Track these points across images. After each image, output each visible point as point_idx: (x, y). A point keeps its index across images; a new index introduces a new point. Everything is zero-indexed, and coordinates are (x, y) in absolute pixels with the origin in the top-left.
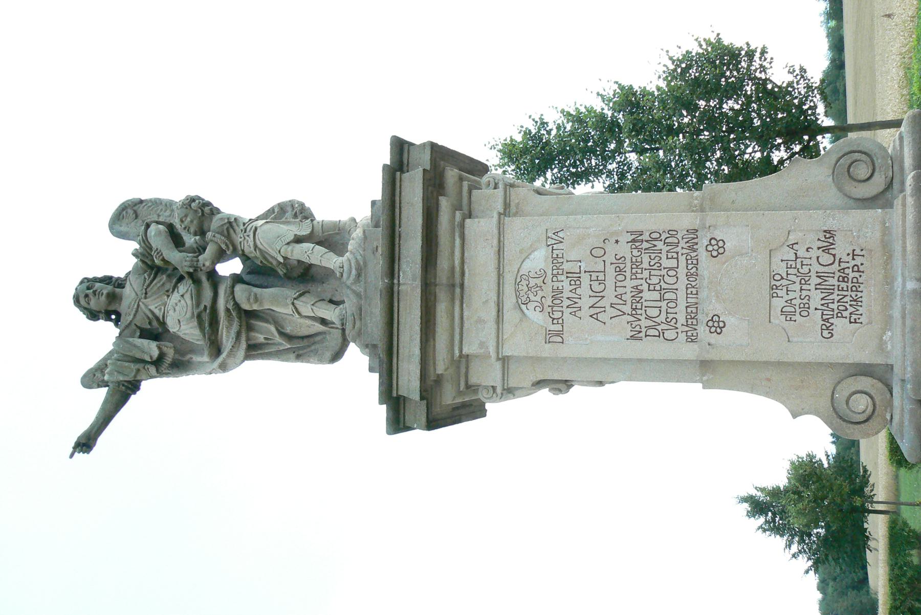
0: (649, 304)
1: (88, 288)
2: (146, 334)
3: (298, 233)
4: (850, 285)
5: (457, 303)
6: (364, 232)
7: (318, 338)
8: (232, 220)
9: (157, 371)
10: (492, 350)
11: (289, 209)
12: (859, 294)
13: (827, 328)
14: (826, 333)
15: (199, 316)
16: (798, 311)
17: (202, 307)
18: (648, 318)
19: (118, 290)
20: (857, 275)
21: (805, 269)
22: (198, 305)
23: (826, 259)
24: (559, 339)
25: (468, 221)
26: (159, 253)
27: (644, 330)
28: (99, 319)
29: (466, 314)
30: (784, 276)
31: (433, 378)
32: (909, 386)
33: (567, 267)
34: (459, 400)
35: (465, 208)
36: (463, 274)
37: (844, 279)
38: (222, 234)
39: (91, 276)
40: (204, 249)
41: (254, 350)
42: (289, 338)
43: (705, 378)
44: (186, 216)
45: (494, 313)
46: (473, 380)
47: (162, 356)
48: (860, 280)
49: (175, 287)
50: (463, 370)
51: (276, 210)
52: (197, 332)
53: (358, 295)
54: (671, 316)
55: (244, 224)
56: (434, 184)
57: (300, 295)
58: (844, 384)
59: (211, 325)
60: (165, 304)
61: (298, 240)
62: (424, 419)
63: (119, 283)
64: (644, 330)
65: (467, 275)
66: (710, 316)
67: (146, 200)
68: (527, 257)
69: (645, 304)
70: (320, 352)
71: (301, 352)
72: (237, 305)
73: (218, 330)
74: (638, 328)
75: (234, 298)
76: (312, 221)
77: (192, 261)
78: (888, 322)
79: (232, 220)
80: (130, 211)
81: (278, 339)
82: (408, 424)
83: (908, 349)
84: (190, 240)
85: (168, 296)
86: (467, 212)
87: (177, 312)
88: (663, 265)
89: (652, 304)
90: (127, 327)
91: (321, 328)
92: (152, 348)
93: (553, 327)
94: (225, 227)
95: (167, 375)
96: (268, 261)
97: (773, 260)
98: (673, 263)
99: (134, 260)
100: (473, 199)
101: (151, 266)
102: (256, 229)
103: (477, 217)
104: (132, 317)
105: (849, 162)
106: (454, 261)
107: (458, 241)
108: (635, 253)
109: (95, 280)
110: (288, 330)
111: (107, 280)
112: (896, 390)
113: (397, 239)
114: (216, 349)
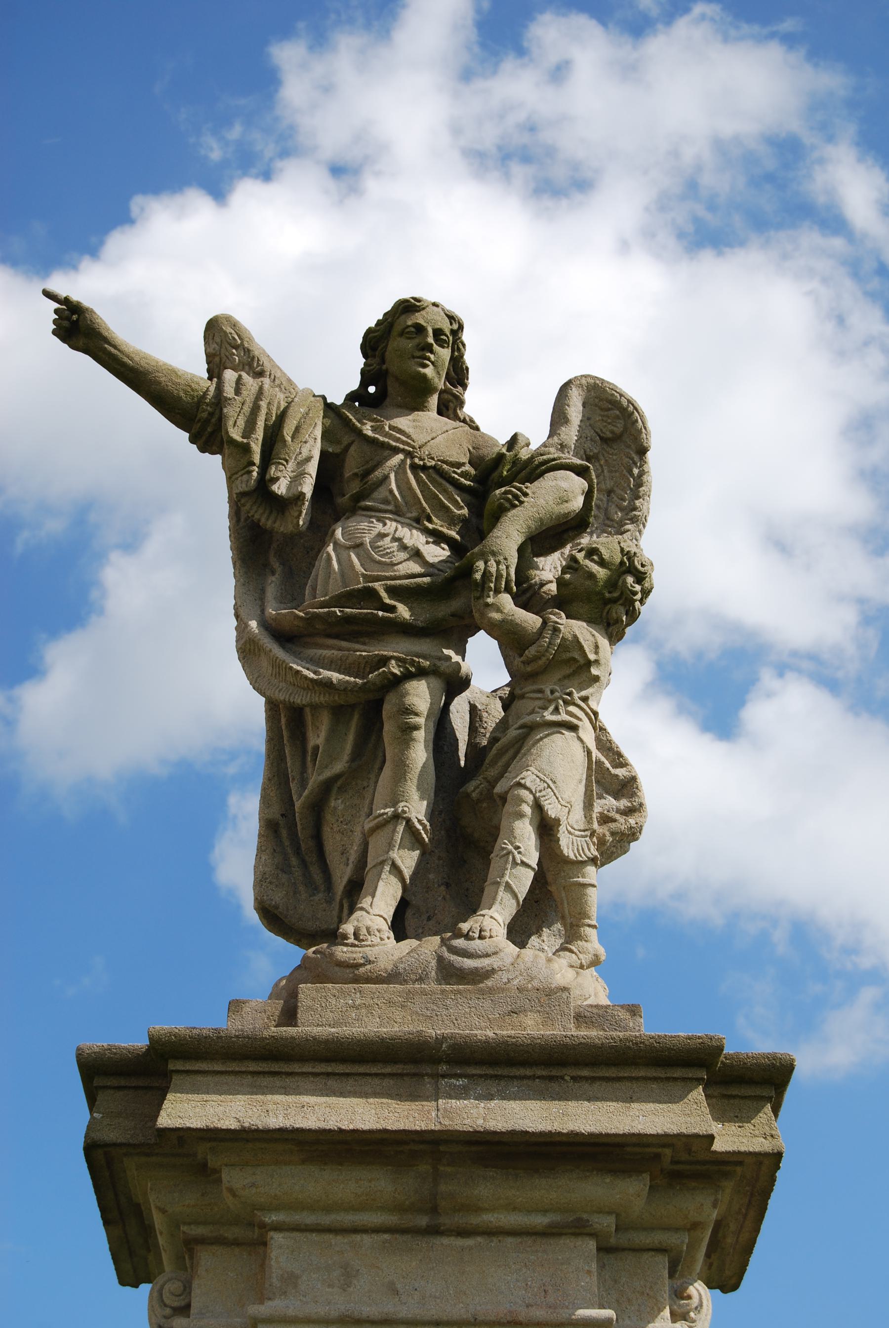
3: (562, 829)
5: (391, 1219)
6: (565, 989)
8: (594, 671)
9: (243, 494)
11: (624, 803)
26: (514, 502)
28: (365, 355)
31: (213, 1162)
34: (158, 1221)
35: (623, 1239)
36: (463, 1233)
40: (525, 606)
42: (318, 807)
44: (602, 563)
46: (206, 1258)
47: (284, 505)
50: (232, 1233)
55: (585, 699)
56: (680, 1164)
61: (546, 829)
62: (111, 1135)
63: (450, 406)
65: (460, 1242)
67: (643, 461)
70: (284, 878)
71: (284, 833)
72: (396, 682)
73: (337, 637)
76: (593, 861)
79: (594, 671)
80: (619, 427)
81: (315, 779)
82: (101, 1097)
84: (549, 569)
86: (613, 1241)
90: (347, 422)
91: (341, 882)
94: (576, 655)
95: (236, 513)
96: (494, 762)
99: (503, 438)
100: (646, 1256)
101: (497, 475)
102: (573, 728)
103: (602, 1267)
106: (492, 1210)
107: (540, 1221)
110: (337, 803)
111: (458, 374)
113: (540, 1072)
114: (286, 636)
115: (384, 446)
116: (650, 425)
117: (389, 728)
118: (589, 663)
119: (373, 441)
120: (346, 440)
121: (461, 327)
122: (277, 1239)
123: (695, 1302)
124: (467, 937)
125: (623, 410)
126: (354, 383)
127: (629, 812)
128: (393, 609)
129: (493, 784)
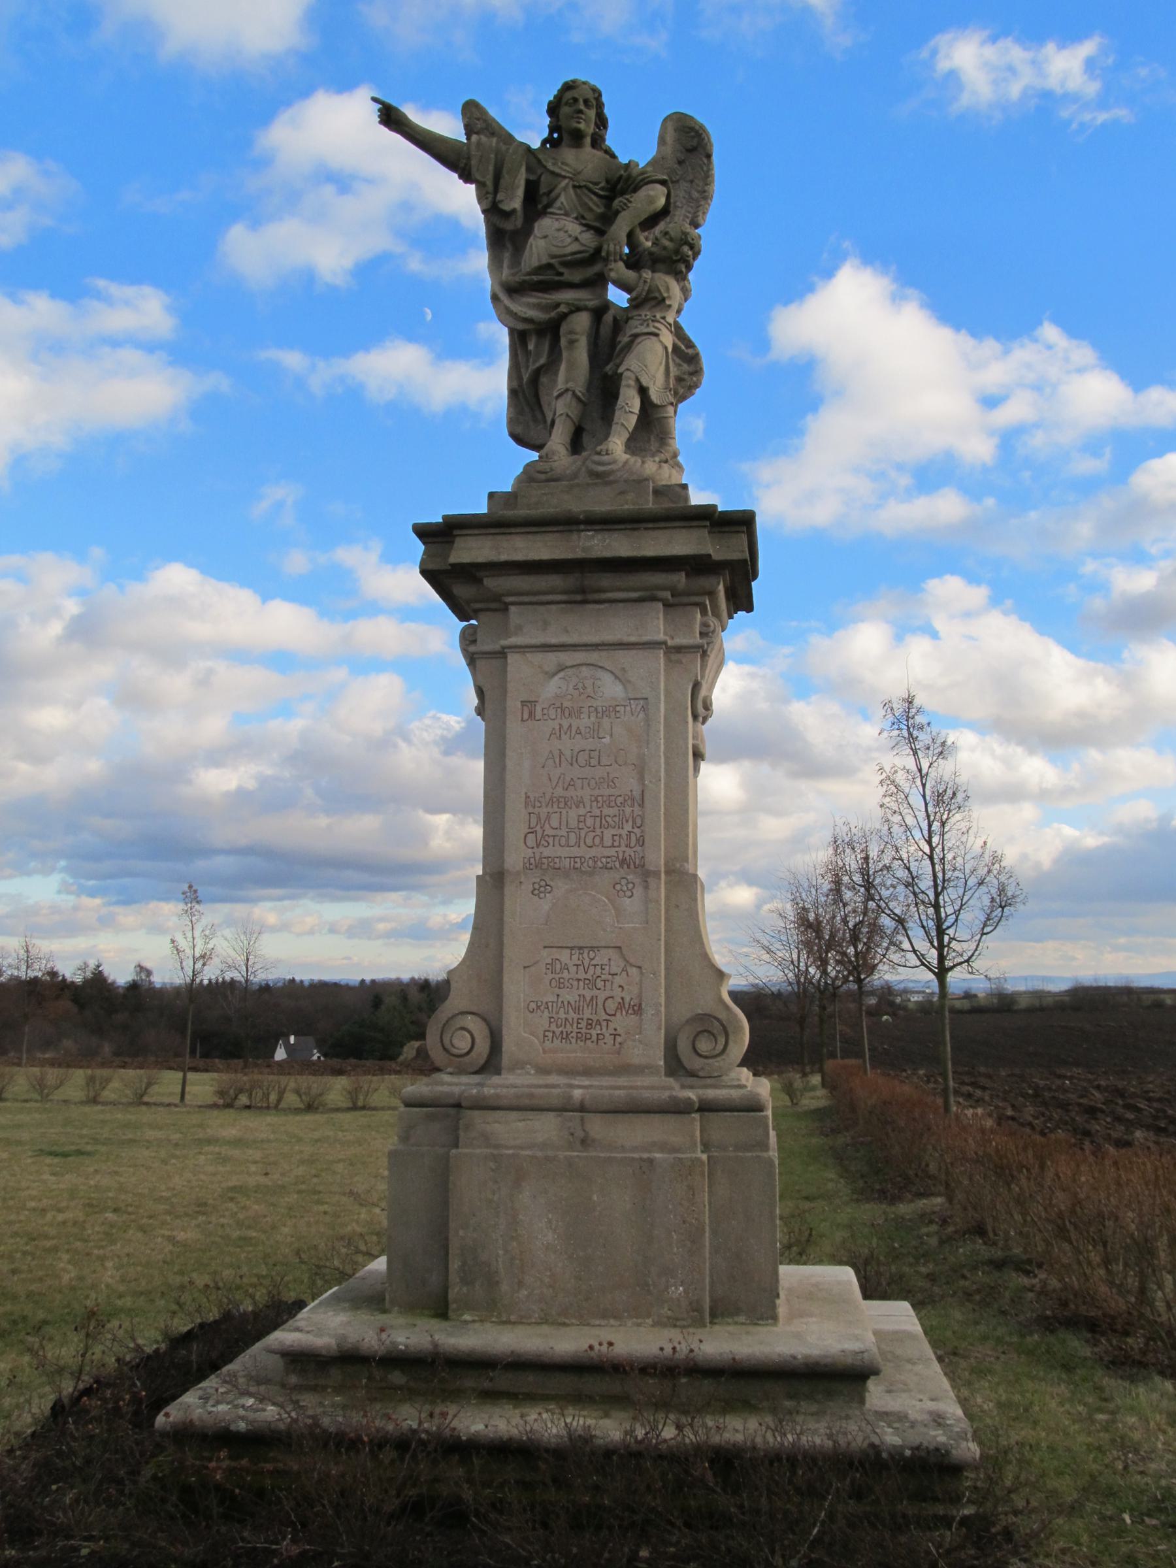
0: (564, 815)
1: (586, 102)
2: (532, 190)
4: (583, 1031)
7: (539, 416)
8: (668, 302)
10: (513, 640)
11: (691, 369)
12: (573, 1041)
13: (538, 1007)
14: (533, 1005)
15: (549, 266)
16: (557, 976)
17: (562, 270)
18: (548, 817)
19: (588, 140)
20: (594, 1038)
21: (600, 984)
22: (565, 264)
23: (611, 1006)
24: (526, 716)
25: (660, 605)
26: (625, 207)
27: (536, 810)
29: (554, 607)
30: (594, 962)
32: (475, 1091)
33: (606, 722)
35: (676, 600)
37: (590, 1025)
38: (649, 291)
39: (604, 99)
41: (519, 339)
43: (488, 878)
44: (671, 240)
45: (554, 641)
47: (507, 215)
48: (588, 1042)
49: (588, 227)
51: (690, 351)
52: (535, 263)
53: (575, 476)
54: (551, 840)
55: (664, 318)
56: (699, 566)
57: (578, 399)
58: (483, 1026)
59: (540, 282)
60: (567, 214)
61: (643, 391)
63: (597, 141)
64: (536, 810)
66: (552, 883)
68: (617, 677)
69: (564, 812)
71: (520, 395)
72: (564, 317)
74: (538, 804)
75: (572, 312)
77: (615, 253)
78: (543, 1070)
79: (668, 302)
80: (695, 142)
83: (513, 1091)
85: (576, 218)
87: (556, 234)
88: (606, 832)
89: (564, 820)
90: (539, 161)
92: (515, 202)
93: (538, 709)
94: (657, 295)
96: (618, 355)
97: (610, 950)
98: (608, 841)
100: (689, 608)
101: (621, 183)
102: (657, 335)
104: (551, 168)
105: (715, 1032)
108: (620, 800)
109: (600, 106)
110: (544, 380)
112: (476, 1079)
113: (629, 526)
114: (513, 290)
115: (558, 175)
116: (713, 140)
117: (563, 342)
118: (664, 299)
119: (553, 173)
120: (539, 172)
121: (600, 95)
122: (512, 609)
123: (712, 628)
124: (599, 453)
125: (697, 132)
126: (545, 134)
127: (692, 374)
128: (561, 274)
129: (618, 366)
